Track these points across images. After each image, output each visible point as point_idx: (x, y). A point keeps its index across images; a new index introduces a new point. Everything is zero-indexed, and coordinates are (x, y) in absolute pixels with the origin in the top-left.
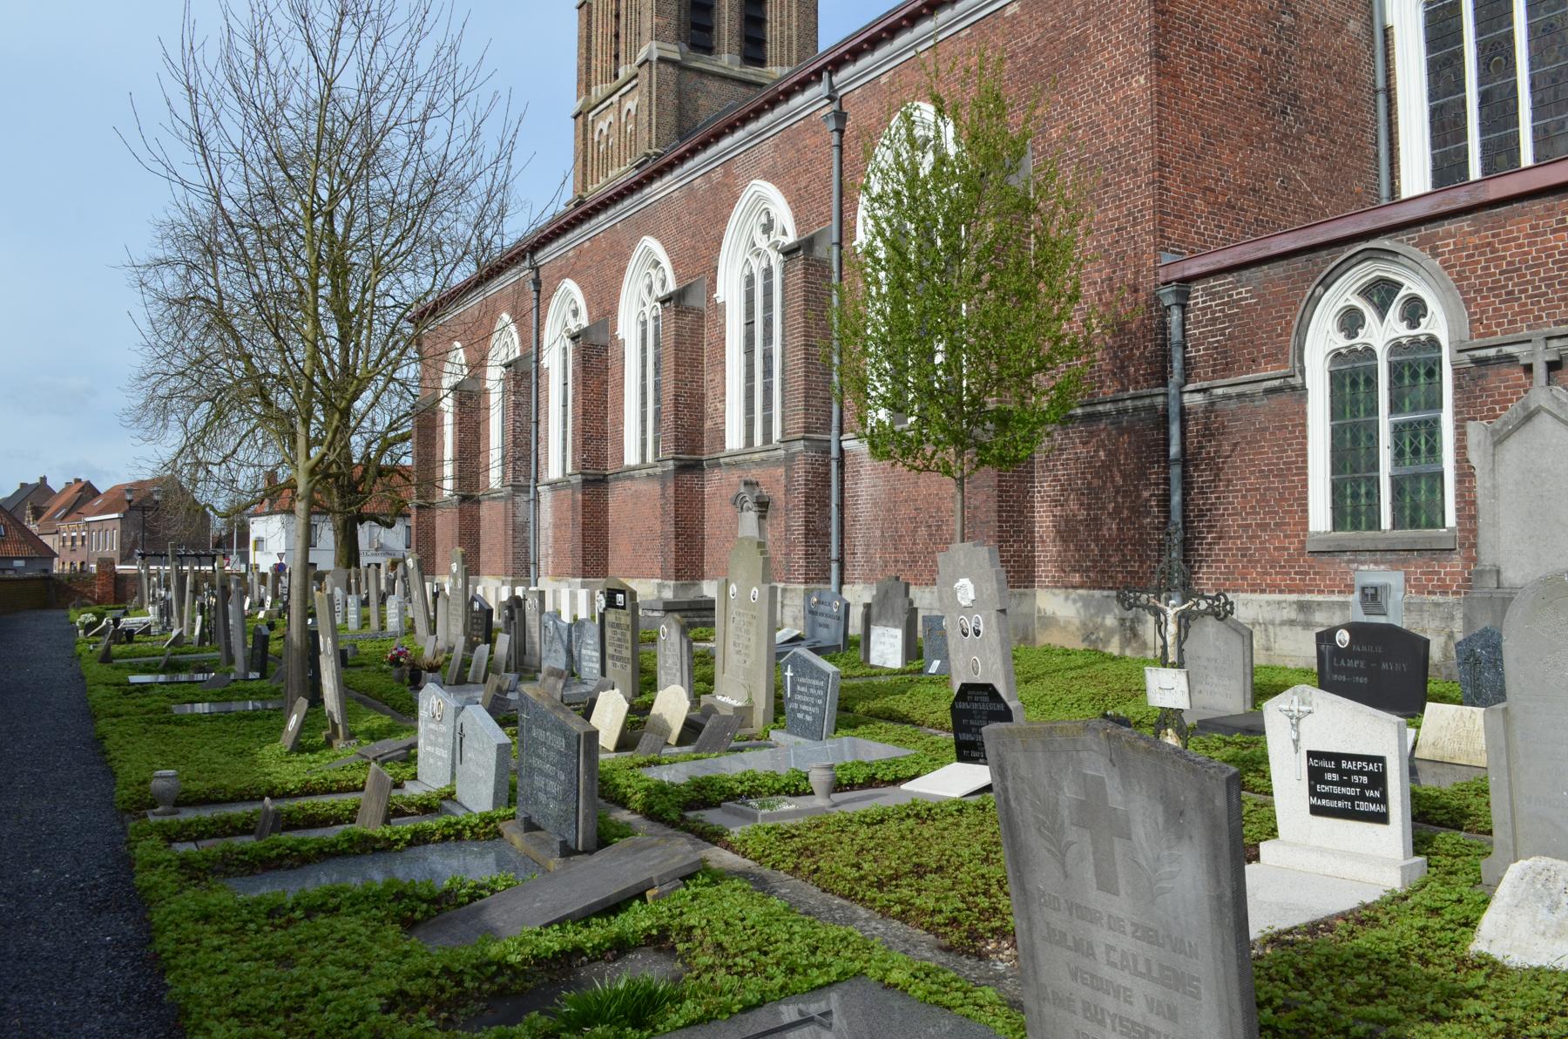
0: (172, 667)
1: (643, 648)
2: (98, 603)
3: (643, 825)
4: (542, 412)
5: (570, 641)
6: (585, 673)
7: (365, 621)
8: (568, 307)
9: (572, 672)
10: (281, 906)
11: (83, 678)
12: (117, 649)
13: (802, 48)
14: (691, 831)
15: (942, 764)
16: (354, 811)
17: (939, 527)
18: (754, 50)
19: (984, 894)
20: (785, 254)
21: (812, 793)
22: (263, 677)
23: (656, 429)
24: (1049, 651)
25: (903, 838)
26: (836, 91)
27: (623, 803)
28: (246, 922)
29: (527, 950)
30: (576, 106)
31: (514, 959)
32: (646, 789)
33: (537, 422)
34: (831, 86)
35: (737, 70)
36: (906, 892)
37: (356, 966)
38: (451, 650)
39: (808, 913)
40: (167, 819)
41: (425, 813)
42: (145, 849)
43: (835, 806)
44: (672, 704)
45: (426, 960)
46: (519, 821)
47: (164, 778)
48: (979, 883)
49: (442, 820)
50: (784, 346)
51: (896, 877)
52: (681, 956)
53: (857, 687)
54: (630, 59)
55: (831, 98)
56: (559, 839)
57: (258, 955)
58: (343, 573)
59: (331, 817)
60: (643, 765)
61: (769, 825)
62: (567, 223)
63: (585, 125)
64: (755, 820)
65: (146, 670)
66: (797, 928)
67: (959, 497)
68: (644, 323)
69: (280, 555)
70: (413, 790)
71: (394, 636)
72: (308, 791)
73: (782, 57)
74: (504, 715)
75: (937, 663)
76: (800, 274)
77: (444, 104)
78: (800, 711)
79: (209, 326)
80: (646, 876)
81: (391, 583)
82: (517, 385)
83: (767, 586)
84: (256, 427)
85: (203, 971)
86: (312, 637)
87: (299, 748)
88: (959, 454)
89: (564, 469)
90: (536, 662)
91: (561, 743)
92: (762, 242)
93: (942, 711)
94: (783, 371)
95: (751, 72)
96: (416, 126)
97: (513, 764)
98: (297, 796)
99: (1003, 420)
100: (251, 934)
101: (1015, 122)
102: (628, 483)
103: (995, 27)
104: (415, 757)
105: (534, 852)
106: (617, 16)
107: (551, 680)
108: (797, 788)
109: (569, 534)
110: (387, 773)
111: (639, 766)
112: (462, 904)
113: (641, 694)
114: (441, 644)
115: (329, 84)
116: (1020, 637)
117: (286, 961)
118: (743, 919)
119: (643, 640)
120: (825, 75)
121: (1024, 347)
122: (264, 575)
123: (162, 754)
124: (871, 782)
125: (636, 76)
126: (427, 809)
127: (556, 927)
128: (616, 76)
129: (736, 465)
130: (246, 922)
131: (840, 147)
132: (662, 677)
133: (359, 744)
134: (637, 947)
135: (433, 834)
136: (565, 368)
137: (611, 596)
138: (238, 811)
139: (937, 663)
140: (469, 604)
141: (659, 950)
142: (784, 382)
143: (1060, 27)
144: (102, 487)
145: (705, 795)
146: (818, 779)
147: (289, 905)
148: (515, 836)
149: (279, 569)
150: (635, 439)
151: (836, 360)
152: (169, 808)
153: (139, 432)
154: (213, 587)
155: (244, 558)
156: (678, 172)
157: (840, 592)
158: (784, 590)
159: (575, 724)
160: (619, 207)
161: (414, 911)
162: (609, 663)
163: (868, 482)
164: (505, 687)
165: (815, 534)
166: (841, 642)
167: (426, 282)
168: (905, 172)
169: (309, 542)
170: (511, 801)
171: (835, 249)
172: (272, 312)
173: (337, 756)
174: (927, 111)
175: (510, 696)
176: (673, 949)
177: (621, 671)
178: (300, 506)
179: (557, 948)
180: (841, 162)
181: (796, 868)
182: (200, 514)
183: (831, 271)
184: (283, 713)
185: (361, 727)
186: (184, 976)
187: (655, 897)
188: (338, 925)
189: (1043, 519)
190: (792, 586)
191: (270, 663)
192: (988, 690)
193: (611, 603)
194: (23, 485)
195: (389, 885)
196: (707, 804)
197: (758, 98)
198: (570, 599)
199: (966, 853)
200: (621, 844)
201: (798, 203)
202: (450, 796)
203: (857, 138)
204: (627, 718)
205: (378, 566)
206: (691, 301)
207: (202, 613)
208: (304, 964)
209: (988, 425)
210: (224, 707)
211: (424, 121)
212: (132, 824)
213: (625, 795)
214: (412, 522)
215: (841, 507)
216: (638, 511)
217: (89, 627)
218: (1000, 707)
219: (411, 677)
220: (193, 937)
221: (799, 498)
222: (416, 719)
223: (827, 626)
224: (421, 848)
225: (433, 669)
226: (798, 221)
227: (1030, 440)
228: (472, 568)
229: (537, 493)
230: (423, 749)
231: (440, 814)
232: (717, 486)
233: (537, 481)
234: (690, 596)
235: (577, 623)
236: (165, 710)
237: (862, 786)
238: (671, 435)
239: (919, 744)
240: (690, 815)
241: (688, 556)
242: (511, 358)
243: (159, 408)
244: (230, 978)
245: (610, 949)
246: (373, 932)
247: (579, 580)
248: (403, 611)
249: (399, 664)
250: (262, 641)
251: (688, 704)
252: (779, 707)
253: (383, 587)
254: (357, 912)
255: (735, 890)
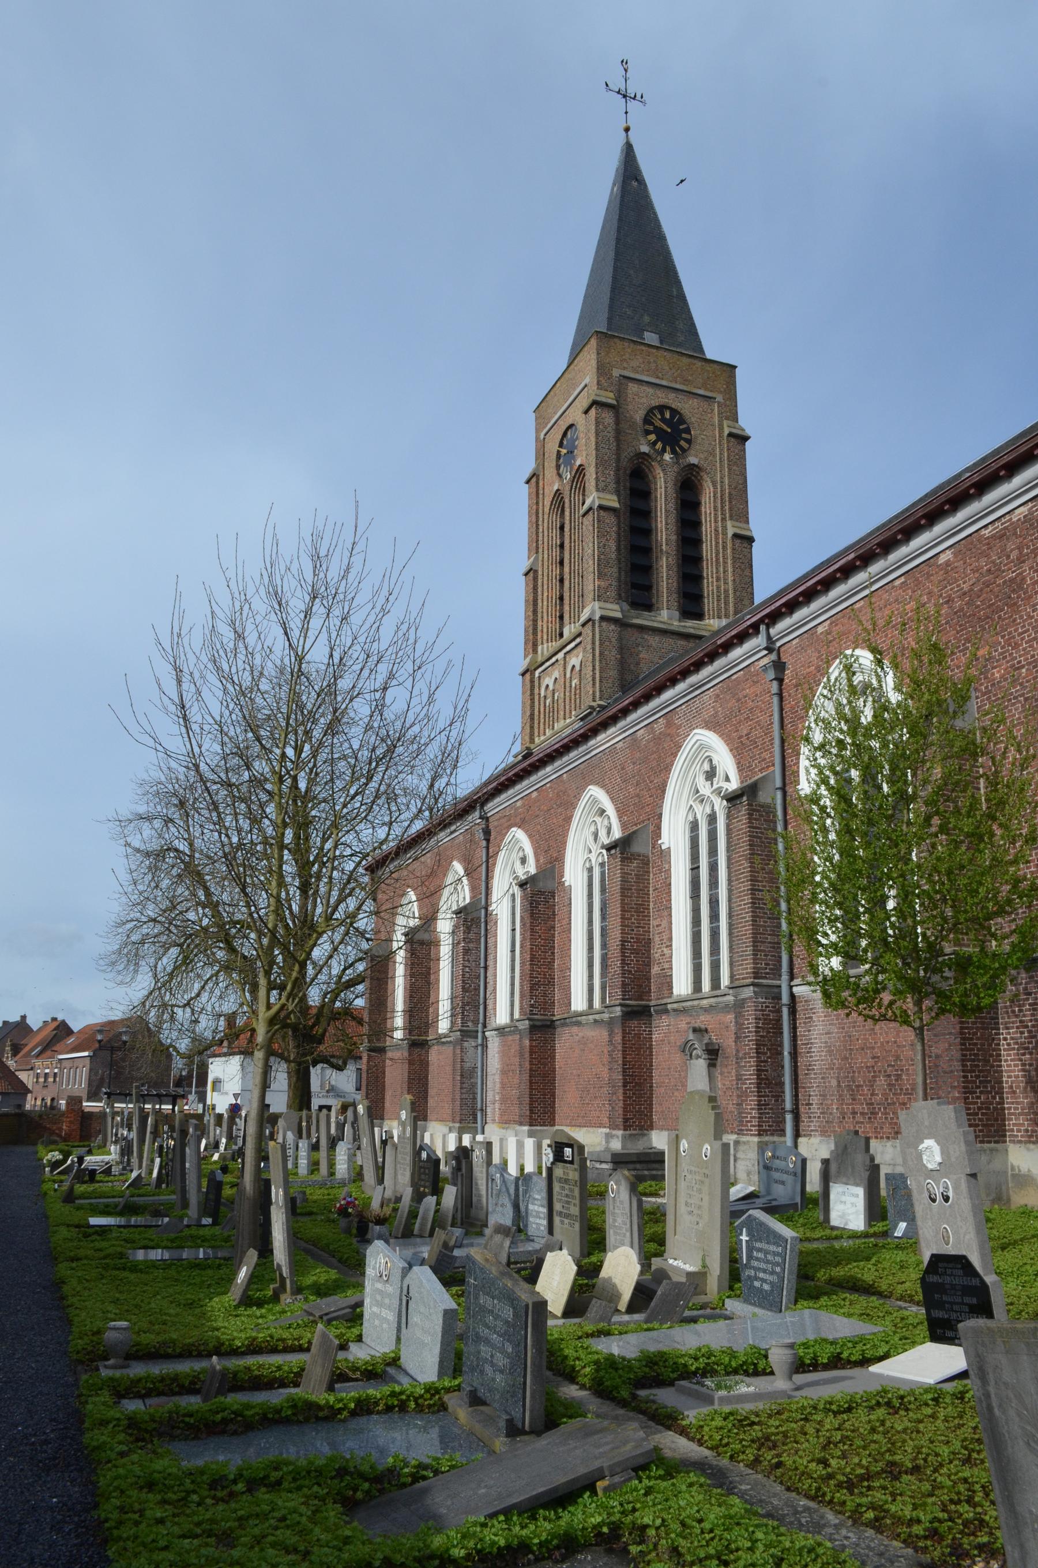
0: (130, 1209)
1: (592, 1203)
2: (65, 1140)
3: (593, 1404)
4: (490, 957)
5: (517, 1195)
6: (532, 1230)
7: (314, 1166)
8: (516, 856)
9: (519, 1228)
10: (224, 1477)
11: (47, 1217)
12: (80, 1188)
13: (739, 600)
14: (643, 1412)
15: (914, 1344)
16: (299, 1374)
17: (898, 1077)
18: (691, 604)
19: (968, 1502)
20: (728, 800)
21: (772, 1373)
22: (215, 1223)
23: (604, 974)
24: (1026, 1212)
25: (873, 1430)
26: (774, 643)
27: (571, 1376)
28: (188, 1493)
29: (471, 1544)
30: (523, 664)
31: (458, 1553)
32: (596, 1363)
33: (486, 968)
34: (769, 637)
35: (676, 625)
36: (879, 1496)
37: (296, 1551)
38: (398, 1199)
39: (769, 1515)
40: (118, 1374)
41: (369, 1379)
42: (98, 1405)
43: (798, 1388)
44: (622, 1267)
45: (367, 1549)
46: (464, 1394)
47: (118, 1329)
48: (962, 1488)
49: (386, 1389)
50: (730, 891)
51: (868, 1477)
52: (634, 1559)
53: (817, 1252)
54: (573, 620)
55: (769, 649)
56: (505, 1417)
57: (199, 1531)
58: (295, 1115)
59: (275, 1379)
60: (592, 1335)
61: (727, 1409)
62: (516, 775)
63: (532, 682)
64: (712, 1403)
65: (105, 1212)
66: (759, 1535)
67: (919, 1047)
68: (590, 870)
69: (236, 1096)
70: (358, 1353)
71: (343, 1183)
72: (254, 1349)
73: (719, 610)
74: (450, 1274)
75: (903, 1225)
76: (745, 819)
77: (404, 672)
78: (756, 1278)
79: (179, 876)
80: (597, 1464)
81: (341, 1127)
82: (468, 930)
83: (718, 1144)
84: (218, 972)
85: (144, 1545)
86: (264, 1187)
87: (247, 1301)
88: (918, 1003)
89: (512, 1014)
90: (482, 1216)
91: (508, 1313)
92: (705, 789)
93: (911, 1281)
94: (730, 916)
95: (690, 626)
96: (378, 695)
97: (460, 1328)
98: (243, 1354)
99: (963, 965)
100: (193, 1506)
101: (956, 667)
102: (575, 1029)
103: (929, 575)
104: (361, 1316)
105: (478, 1428)
106: (562, 581)
107: (498, 1238)
108: (755, 1366)
109: (516, 1081)
110: (332, 1333)
111: (589, 1335)
112: (404, 1485)
113: (589, 1254)
114: (389, 1194)
115: (300, 659)
116: (992, 1196)
117: (226, 1539)
118: (700, 1521)
119: (591, 1194)
120: (762, 628)
121: (982, 890)
122: (220, 1116)
123: (115, 1301)
124: (836, 1362)
125: (579, 635)
126: (372, 1374)
127: (502, 1518)
128: (561, 635)
129: (684, 1011)
130: (188, 1493)
131: (780, 695)
132: (611, 1238)
133: (306, 1299)
134: (586, 1546)
135: (377, 1403)
136: (513, 914)
137: (558, 1148)
138: (184, 1367)
139: (903, 1225)
140: (417, 1153)
141: (610, 1551)
142: (731, 926)
143: (996, 571)
144: (76, 1026)
145: (659, 1371)
146: (779, 1357)
147: (232, 1477)
148: (461, 1412)
149: (235, 1109)
150: (582, 986)
151: (784, 906)
152: (120, 1361)
153: (110, 976)
154: (172, 1129)
155: (202, 1097)
156: (621, 724)
157: (796, 1146)
158: (737, 1143)
159: (522, 1292)
160: (565, 759)
161: (355, 1489)
162: (557, 1220)
163: (822, 1032)
164: (452, 1243)
165: (768, 1084)
166: (798, 1200)
167: (382, 833)
168: (847, 721)
169: (265, 1085)
170: (457, 1372)
171: (779, 795)
172: (237, 863)
173: (284, 1312)
174: (865, 657)
175: (457, 1253)
176: (625, 1551)
177: (568, 1230)
178: (259, 1055)
179: (502, 1543)
180: (781, 709)
181: (757, 1461)
182: (164, 1052)
183: (775, 816)
184: (232, 1264)
185: (309, 1280)
186: (125, 1549)
187: (606, 1489)
188: (280, 1503)
189: (1012, 1069)
190: (744, 1139)
191: (222, 1209)
192: (962, 1262)
193: (559, 1157)
194: (5, 1023)
195: (332, 1459)
196: (660, 1382)
197: (698, 652)
198: (517, 1149)
199: (945, 1451)
200: (570, 1425)
201: (739, 750)
202: (394, 1361)
203: (796, 686)
204: (575, 1280)
205: (329, 1108)
206: (636, 848)
207: (160, 1156)
208: (244, 1545)
209: (947, 973)
210: (176, 1254)
211: (385, 689)
212: (84, 1377)
213: (573, 1367)
214: (363, 1064)
215: (794, 1055)
216: (585, 1058)
217: (55, 1165)
218: (975, 1282)
219: (359, 1229)
220: (137, 1506)
221: (749, 1045)
222: (363, 1274)
223: (783, 1183)
224: (365, 1419)
225: (381, 1221)
226: (740, 768)
227: (992, 986)
228: (420, 1114)
229: (485, 1038)
230: (369, 1309)
231: (387, 1383)
232: (666, 1032)
233: (485, 1026)
234: (638, 1147)
235: (524, 1178)
236: (122, 1255)
237: (826, 1367)
238: (618, 981)
239: (888, 1318)
240: (642, 1393)
241: (636, 1107)
242: (462, 905)
243: (130, 955)
244: (171, 1556)
245: (558, 1547)
246: (314, 1512)
247: (526, 1128)
248: (352, 1157)
249: (347, 1215)
250: (216, 1186)
251: (638, 1268)
252: (734, 1274)
253: (333, 1131)
254: (299, 1488)
255: (691, 1485)
